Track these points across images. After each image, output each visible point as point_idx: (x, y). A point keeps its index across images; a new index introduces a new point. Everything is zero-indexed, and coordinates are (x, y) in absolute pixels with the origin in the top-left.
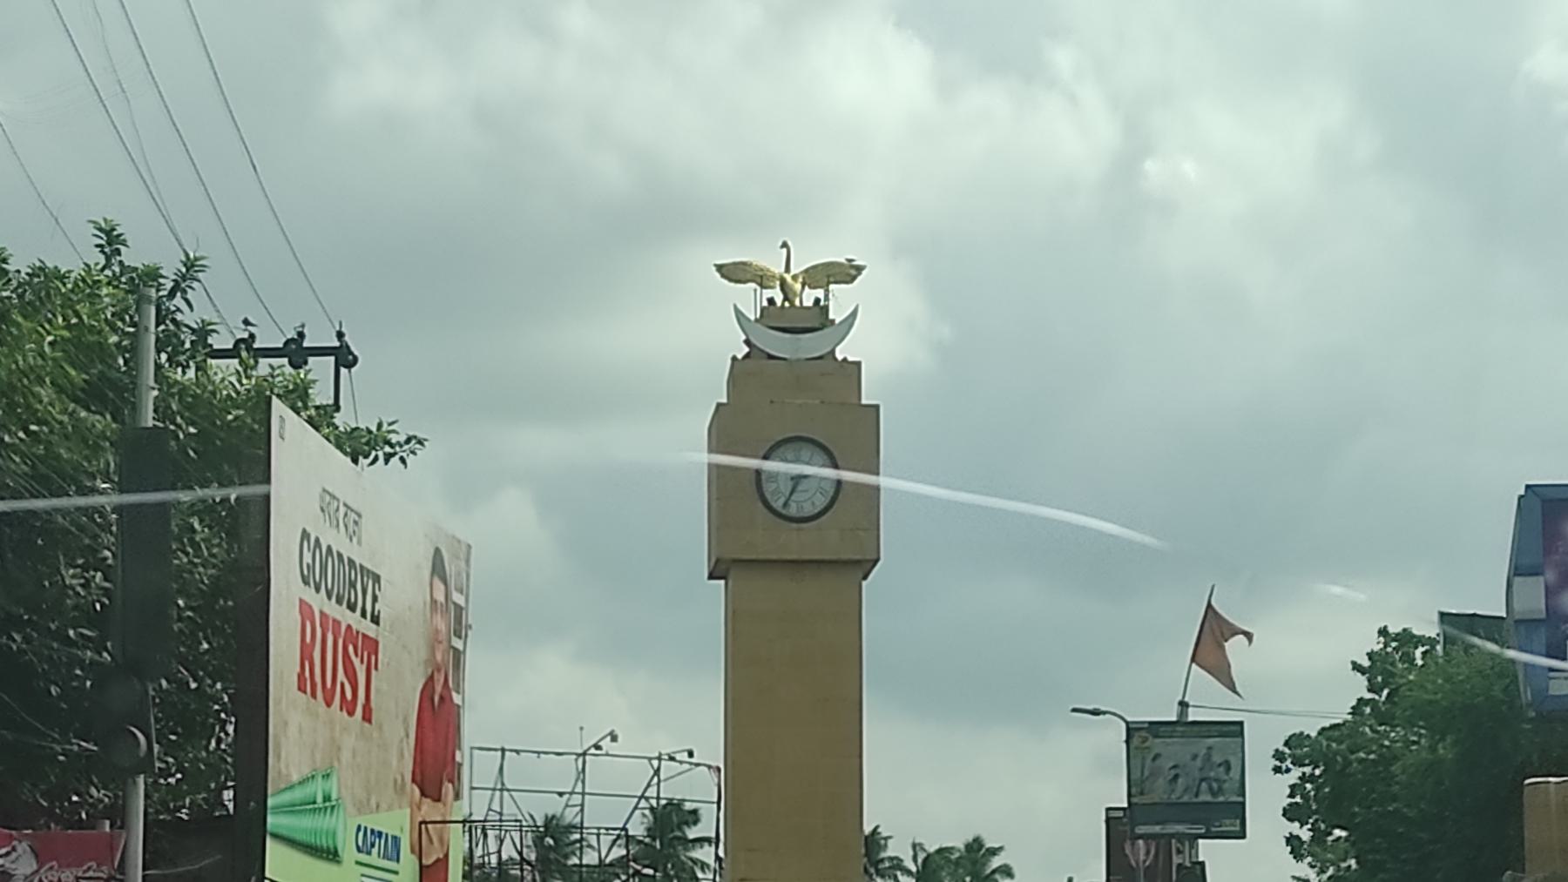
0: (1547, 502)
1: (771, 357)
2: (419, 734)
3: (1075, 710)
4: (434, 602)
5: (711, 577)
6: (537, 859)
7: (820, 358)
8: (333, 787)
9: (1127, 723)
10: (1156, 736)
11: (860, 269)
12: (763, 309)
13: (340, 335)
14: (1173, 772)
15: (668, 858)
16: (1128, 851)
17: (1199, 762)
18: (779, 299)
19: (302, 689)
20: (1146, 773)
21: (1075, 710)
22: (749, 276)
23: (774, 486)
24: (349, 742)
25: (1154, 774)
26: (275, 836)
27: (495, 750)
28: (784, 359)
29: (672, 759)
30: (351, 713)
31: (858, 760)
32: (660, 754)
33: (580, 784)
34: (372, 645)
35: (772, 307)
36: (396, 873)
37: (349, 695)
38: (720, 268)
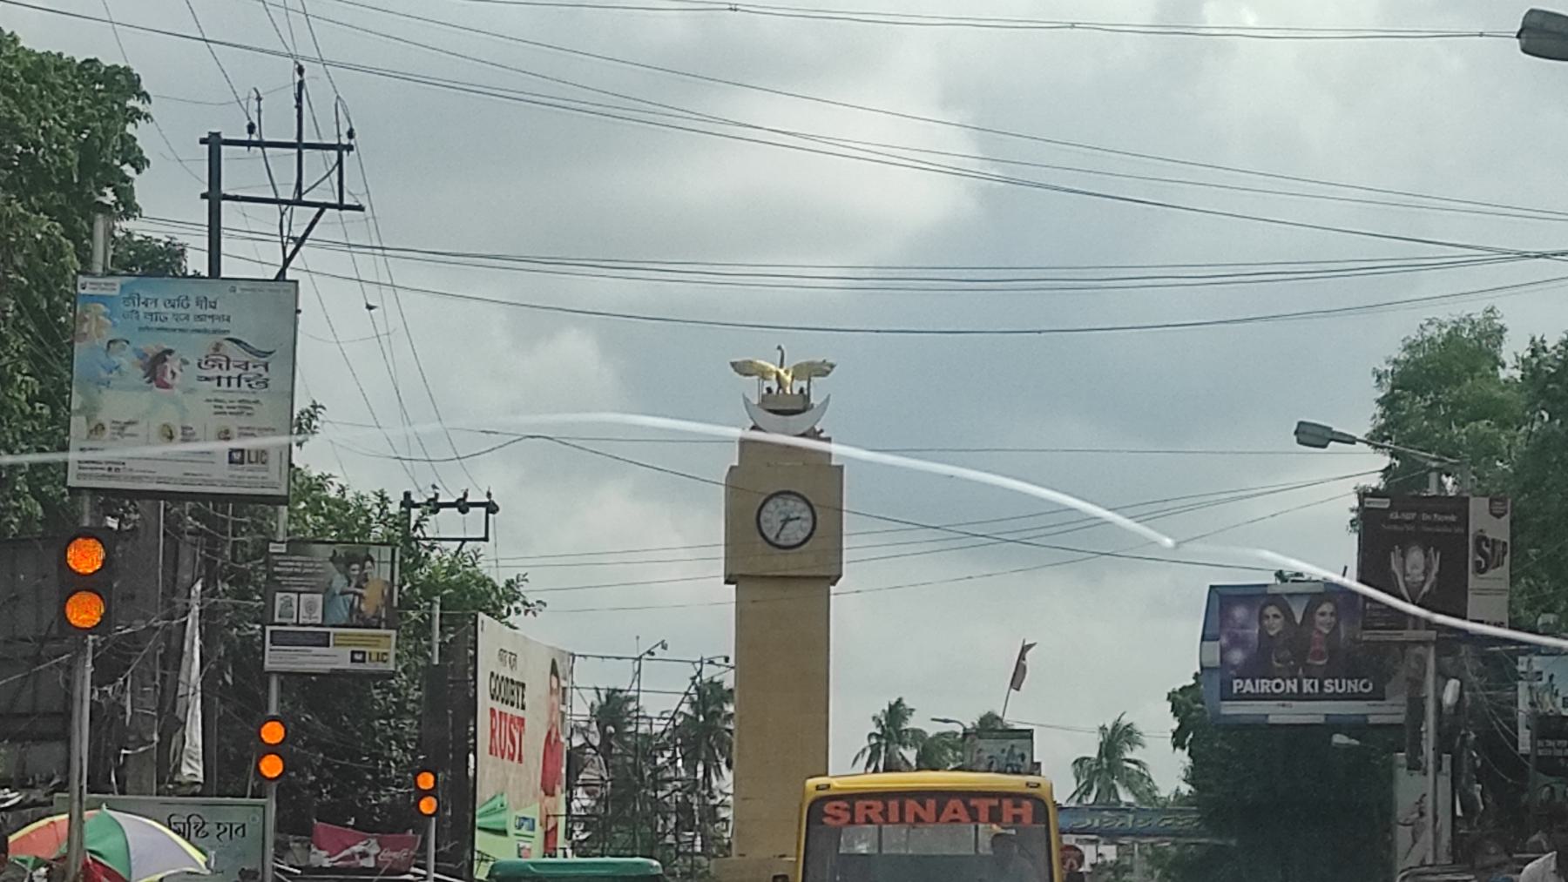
0: (1222, 597)
2: (549, 768)
3: (933, 720)
4: (551, 688)
5: (727, 582)
6: (600, 745)
8: (505, 800)
10: (980, 738)
11: (832, 366)
12: (763, 396)
13: (489, 495)
14: (990, 761)
16: (1394, 567)
17: (1005, 755)
18: (775, 388)
19: (491, 753)
20: (974, 759)
21: (933, 720)
22: (754, 371)
23: (769, 525)
24: (512, 776)
26: (480, 828)
29: (711, 662)
30: (513, 759)
31: (824, 716)
33: (636, 683)
34: (522, 721)
36: (532, 837)
37: (512, 751)
38: (733, 364)
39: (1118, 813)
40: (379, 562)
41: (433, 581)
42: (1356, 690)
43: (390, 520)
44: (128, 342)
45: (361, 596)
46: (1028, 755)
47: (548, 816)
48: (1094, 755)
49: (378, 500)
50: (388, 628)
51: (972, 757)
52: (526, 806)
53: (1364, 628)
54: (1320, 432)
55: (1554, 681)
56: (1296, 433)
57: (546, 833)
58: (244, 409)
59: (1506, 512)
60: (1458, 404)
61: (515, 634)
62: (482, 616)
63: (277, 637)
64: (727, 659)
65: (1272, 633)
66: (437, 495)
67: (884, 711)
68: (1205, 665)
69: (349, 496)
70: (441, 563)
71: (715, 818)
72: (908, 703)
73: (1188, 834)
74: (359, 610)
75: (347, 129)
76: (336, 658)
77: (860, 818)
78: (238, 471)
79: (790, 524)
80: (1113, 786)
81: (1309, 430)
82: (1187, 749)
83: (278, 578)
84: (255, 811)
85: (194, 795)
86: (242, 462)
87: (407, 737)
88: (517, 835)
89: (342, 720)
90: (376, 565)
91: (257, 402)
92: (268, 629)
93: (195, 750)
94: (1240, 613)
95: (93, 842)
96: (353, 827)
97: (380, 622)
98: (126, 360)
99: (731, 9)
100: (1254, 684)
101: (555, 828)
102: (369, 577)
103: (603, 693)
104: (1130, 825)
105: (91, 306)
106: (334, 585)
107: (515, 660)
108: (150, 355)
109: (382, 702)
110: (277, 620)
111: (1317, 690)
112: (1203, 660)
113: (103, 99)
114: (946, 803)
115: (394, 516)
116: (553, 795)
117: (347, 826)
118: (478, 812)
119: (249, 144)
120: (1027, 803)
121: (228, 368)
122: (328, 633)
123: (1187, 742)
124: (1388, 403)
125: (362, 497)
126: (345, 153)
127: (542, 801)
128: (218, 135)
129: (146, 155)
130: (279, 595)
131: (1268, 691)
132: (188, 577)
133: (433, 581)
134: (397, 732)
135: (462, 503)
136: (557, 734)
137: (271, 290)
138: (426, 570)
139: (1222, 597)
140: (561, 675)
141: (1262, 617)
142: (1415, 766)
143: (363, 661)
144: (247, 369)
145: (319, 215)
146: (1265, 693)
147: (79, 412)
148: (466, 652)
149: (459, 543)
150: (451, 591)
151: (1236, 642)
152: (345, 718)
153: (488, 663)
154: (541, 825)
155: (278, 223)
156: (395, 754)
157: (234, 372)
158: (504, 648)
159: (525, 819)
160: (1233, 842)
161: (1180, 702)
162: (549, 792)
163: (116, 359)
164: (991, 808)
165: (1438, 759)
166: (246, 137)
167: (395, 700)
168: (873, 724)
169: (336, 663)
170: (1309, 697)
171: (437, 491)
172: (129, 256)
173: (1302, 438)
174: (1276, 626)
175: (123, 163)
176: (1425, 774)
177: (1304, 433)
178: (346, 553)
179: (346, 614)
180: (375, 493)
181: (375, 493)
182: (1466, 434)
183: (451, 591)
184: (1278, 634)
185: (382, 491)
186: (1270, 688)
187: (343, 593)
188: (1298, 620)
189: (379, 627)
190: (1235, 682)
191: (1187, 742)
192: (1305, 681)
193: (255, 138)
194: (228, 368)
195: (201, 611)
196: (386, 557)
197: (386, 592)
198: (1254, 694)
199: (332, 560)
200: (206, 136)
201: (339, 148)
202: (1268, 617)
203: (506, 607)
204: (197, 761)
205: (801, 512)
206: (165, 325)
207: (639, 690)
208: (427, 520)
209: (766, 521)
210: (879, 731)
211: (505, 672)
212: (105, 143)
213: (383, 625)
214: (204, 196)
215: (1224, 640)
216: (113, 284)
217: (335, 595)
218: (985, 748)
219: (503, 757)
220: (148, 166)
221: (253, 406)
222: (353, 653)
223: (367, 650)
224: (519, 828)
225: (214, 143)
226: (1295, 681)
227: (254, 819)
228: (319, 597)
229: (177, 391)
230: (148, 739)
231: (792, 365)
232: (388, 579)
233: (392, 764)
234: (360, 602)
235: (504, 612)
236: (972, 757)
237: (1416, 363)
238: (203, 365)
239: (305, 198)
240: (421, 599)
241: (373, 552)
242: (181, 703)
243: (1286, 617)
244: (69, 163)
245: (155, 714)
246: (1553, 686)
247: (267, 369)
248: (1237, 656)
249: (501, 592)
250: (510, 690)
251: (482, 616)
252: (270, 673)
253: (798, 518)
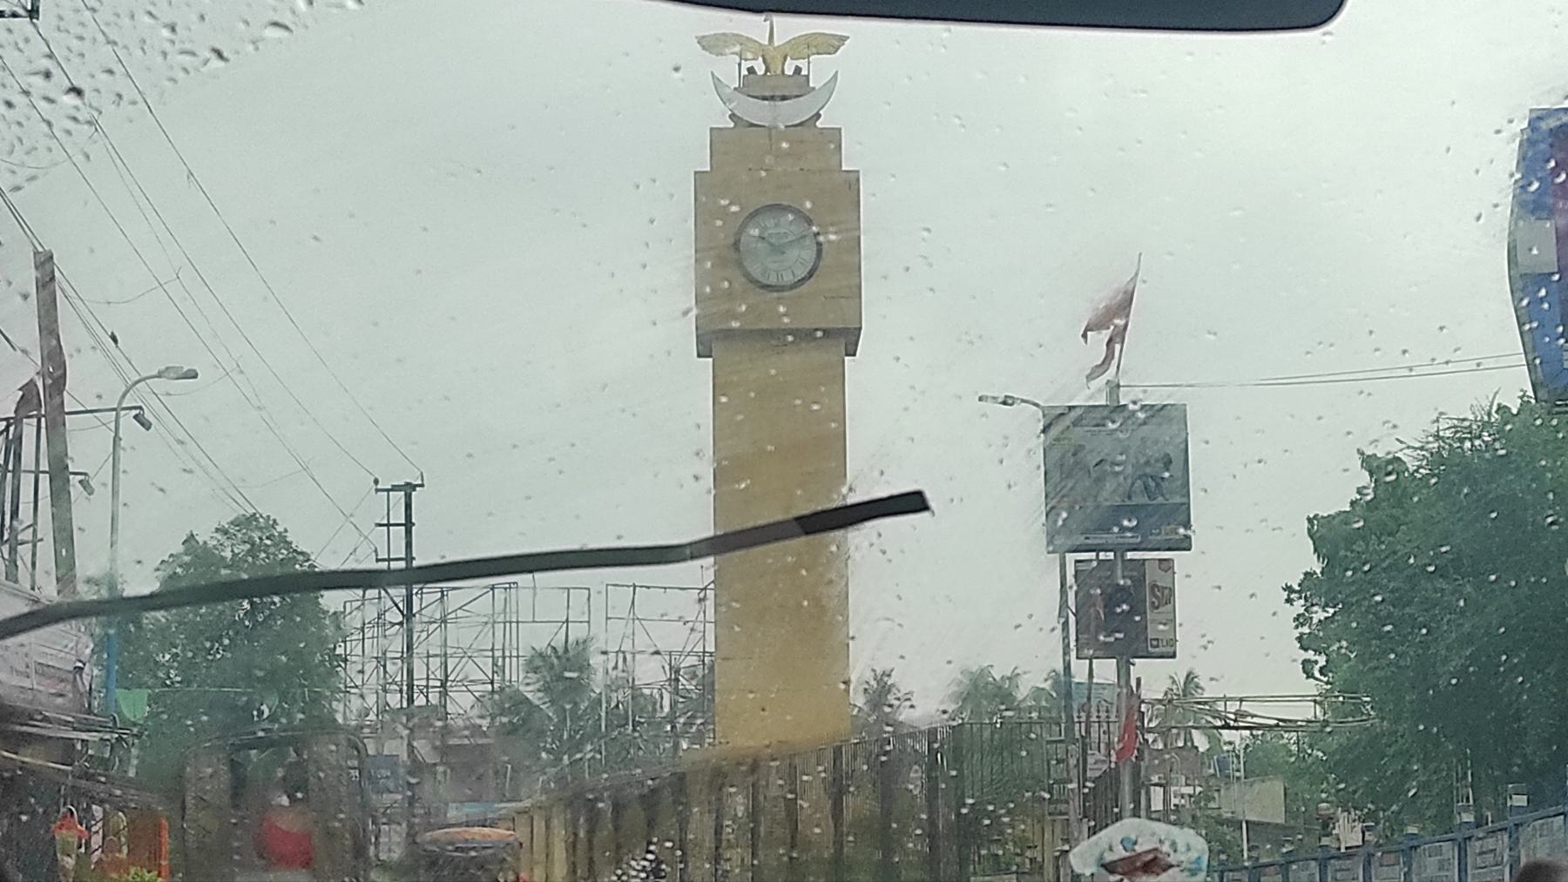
1: (752, 125)
7: (801, 124)
9: (1043, 409)
18: (760, 69)
27: (628, 586)
28: (764, 126)
33: (702, 614)
35: (752, 76)
95: (1055, 558)
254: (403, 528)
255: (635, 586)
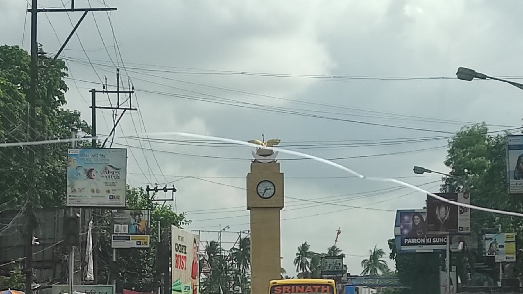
4: (194, 247)
5: (248, 209)
6: (209, 260)
13: (173, 186)
15: (246, 253)
17: (334, 263)
19: (176, 267)
20: (325, 265)
24: (182, 274)
25: (326, 265)
27: (198, 231)
29: (244, 233)
32: (241, 231)
33: (220, 240)
34: (185, 257)
36: (189, 292)
37: (182, 266)
39: (373, 279)
40: (144, 215)
41: (157, 215)
42: (443, 242)
43: (144, 196)
44: (82, 167)
45: (139, 225)
46: (341, 264)
47: (194, 286)
48: (368, 259)
49: (140, 190)
50: (147, 234)
51: (324, 264)
52: (187, 283)
53: (429, 231)
54: (421, 169)
55: (496, 240)
56: (414, 170)
57: (193, 291)
58: (113, 184)
59: (468, 197)
60: (473, 152)
61: (183, 231)
62: (173, 226)
63: (115, 238)
64: (249, 231)
65: (417, 224)
66: (157, 187)
67: (301, 246)
68: (396, 234)
69: (130, 188)
70: (159, 209)
71: (246, 282)
72: (308, 243)
73: (396, 286)
74: (139, 229)
75: (132, 86)
76: (132, 244)
77: (284, 291)
78: (112, 201)
79: (267, 191)
80: (376, 269)
81: (418, 169)
82: (395, 260)
83: (115, 220)
84: (110, 289)
85: (91, 284)
86: (113, 199)
87: (150, 263)
88: (184, 292)
89: (130, 259)
90: (143, 216)
91: (116, 182)
92: (112, 235)
93: (91, 271)
94: (406, 218)
96: (134, 290)
97: (145, 233)
98: (81, 171)
99: (242, 74)
100: (411, 240)
101: (196, 289)
102: (141, 219)
103: (209, 243)
104: (377, 283)
105: (72, 158)
106: (131, 221)
107: (183, 239)
108: (88, 170)
109: (143, 253)
110: (115, 232)
111: (431, 242)
112: (396, 233)
113: (54, 70)
114: (307, 287)
115: (145, 195)
116: (195, 279)
117: (132, 290)
118: (173, 285)
119: (103, 92)
120: (328, 287)
121: (109, 173)
122: (130, 236)
123: (395, 257)
124: (451, 152)
125: (135, 189)
126: (131, 94)
127: (192, 281)
128: (94, 89)
129: (68, 86)
130: (115, 225)
131: (416, 242)
132: (88, 220)
133: (157, 215)
134: (147, 261)
135: (165, 189)
136: (196, 261)
137: (119, 152)
138: (155, 211)
139: (401, 213)
140: (197, 243)
141: (413, 219)
142: (444, 270)
143: (140, 244)
144: (114, 173)
145: (124, 112)
146: (415, 243)
147: (69, 186)
148: (168, 237)
149: (164, 201)
150: (163, 217)
151: (405, 227)
152: (131, 258)
153: (175, 240)
154: (192, 288)
155: (112, 114)
156: (147, 268)
157: (111, 174)
158: (180, 235)
159: (187, 287)
160: (410, 288)
161: (392, 244)
162: (194, 278)
163: (79, 172)
164: (319, 288)
165: (450, 268)
166: (102, 90)
167: (147, 252)
168: (297, 250)
169: (132, 245)
170: (428, 244)
171: (157, 185)
172: (63, 116)
173: (416, 171)
174: (418, 222)
175: (60, 89)
176: (447, 272)
177: (416, 170)
178: (135, 213)
179: (135, 230)
180: (139, 188)
181: (139, 188)
182: (475, 161)
183: (163, 217)
184: (419, 224)
185: (141, 187)
186: (416, 241)
187: (134, 224)
188: (425, 220)
189: (144, 234)
190: (405, 240)
191: (395, 257)
192: (427, 239)
193: (105, 90)
194: (109, 173)
195: (92, 230)
196: (146, 213)
197: (146, 223)
198: (412, 243)
199: (130, 214)
200: (91, 90)
201: (130, 92)
202: (415, 219)
203: (180, 222)
204: (92, 274)
205: (271, 186)
206: (92, 162)
207: (221, 242)
208: (155, 196)
209: (260, 190)
210: (299, 253)
211: (180, 243)
212: (55, 84)
213: (146, 233)
214: (90, 107)
215: (402, 227)
216: (78, 151)
217: (131, 225)
218: (328, 261)
219: (180, 268)
220: (69, 90)
221: (116, 183)
222: (137, 242)
223: (141, 241)
224: (185, 289)
225: (93, 92)
226: (424, 239)
227: (109, 291)
228: (127, 226)
229: (95, 180)
230: (78, 268)
231: (267, 141)
232: (147, 219)
233: (146, 271)
234: (139, 227)
235: (179, 223)
236: (324, 264)
237: (460, 139)
238: (102, 173)
239: (120, 107)
240: (154, 220)
241: (143, 212)
242: (87, 257)
243: (421, 220)
244: (44, 91)
245: (80, 261)
246: (496, 242)
247: (119, 173)
248: (406, 232)
249: (178, 217)
250: (182, 248)
251: (173, 226)
252: (113, 248)
253: (270, 189)
254: (96, 105)
255: (199, 231)
